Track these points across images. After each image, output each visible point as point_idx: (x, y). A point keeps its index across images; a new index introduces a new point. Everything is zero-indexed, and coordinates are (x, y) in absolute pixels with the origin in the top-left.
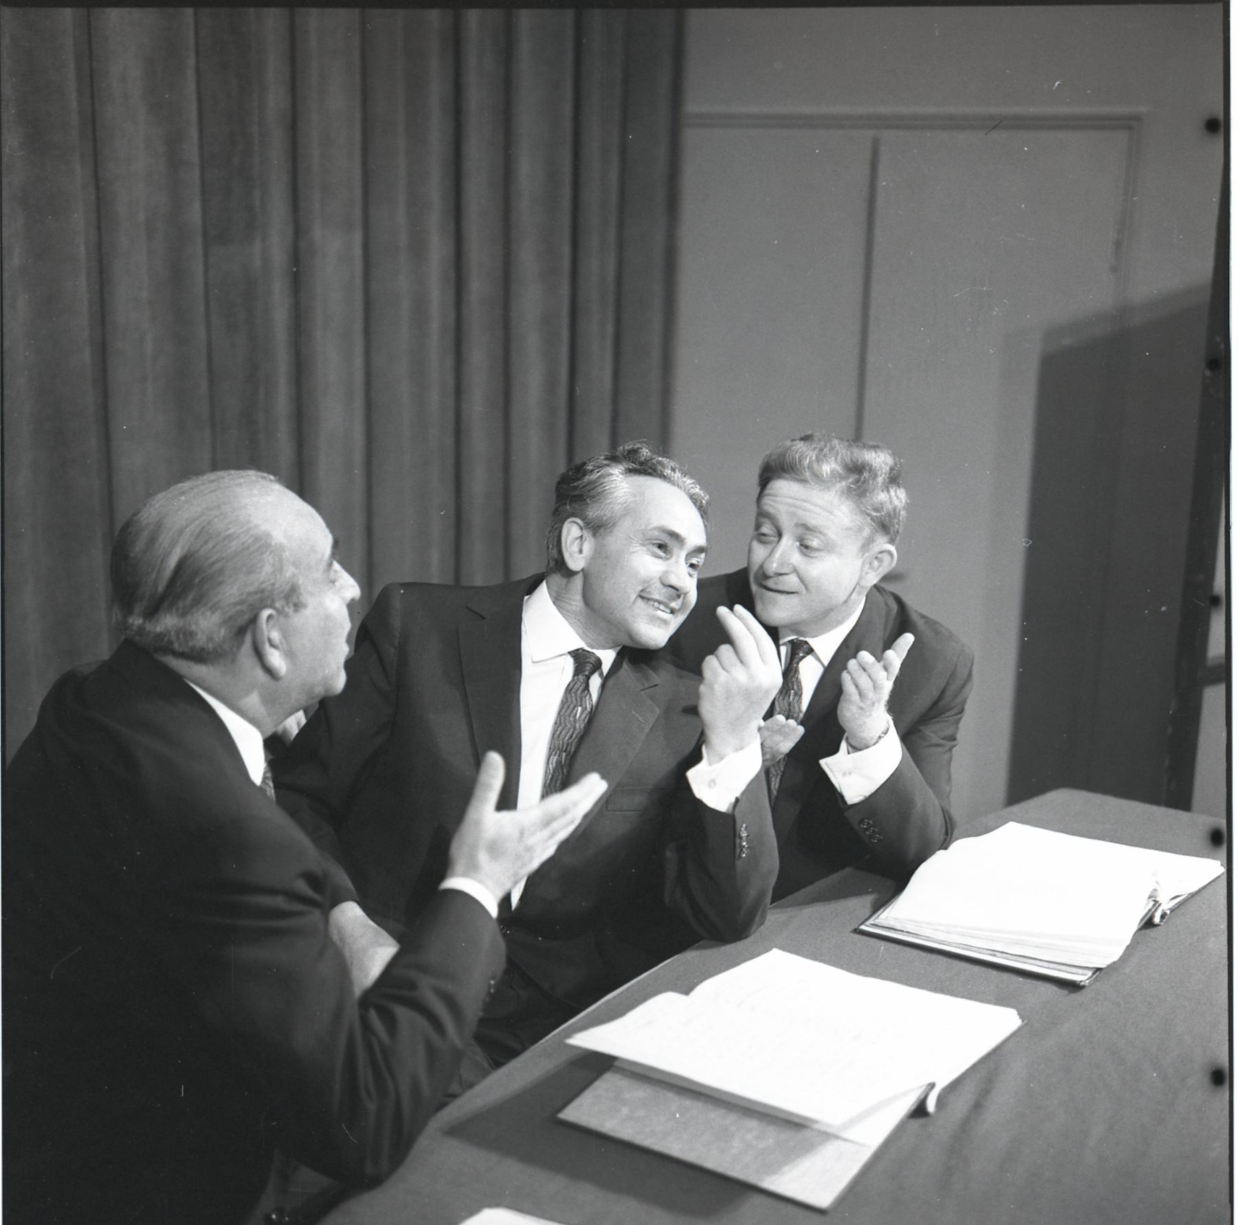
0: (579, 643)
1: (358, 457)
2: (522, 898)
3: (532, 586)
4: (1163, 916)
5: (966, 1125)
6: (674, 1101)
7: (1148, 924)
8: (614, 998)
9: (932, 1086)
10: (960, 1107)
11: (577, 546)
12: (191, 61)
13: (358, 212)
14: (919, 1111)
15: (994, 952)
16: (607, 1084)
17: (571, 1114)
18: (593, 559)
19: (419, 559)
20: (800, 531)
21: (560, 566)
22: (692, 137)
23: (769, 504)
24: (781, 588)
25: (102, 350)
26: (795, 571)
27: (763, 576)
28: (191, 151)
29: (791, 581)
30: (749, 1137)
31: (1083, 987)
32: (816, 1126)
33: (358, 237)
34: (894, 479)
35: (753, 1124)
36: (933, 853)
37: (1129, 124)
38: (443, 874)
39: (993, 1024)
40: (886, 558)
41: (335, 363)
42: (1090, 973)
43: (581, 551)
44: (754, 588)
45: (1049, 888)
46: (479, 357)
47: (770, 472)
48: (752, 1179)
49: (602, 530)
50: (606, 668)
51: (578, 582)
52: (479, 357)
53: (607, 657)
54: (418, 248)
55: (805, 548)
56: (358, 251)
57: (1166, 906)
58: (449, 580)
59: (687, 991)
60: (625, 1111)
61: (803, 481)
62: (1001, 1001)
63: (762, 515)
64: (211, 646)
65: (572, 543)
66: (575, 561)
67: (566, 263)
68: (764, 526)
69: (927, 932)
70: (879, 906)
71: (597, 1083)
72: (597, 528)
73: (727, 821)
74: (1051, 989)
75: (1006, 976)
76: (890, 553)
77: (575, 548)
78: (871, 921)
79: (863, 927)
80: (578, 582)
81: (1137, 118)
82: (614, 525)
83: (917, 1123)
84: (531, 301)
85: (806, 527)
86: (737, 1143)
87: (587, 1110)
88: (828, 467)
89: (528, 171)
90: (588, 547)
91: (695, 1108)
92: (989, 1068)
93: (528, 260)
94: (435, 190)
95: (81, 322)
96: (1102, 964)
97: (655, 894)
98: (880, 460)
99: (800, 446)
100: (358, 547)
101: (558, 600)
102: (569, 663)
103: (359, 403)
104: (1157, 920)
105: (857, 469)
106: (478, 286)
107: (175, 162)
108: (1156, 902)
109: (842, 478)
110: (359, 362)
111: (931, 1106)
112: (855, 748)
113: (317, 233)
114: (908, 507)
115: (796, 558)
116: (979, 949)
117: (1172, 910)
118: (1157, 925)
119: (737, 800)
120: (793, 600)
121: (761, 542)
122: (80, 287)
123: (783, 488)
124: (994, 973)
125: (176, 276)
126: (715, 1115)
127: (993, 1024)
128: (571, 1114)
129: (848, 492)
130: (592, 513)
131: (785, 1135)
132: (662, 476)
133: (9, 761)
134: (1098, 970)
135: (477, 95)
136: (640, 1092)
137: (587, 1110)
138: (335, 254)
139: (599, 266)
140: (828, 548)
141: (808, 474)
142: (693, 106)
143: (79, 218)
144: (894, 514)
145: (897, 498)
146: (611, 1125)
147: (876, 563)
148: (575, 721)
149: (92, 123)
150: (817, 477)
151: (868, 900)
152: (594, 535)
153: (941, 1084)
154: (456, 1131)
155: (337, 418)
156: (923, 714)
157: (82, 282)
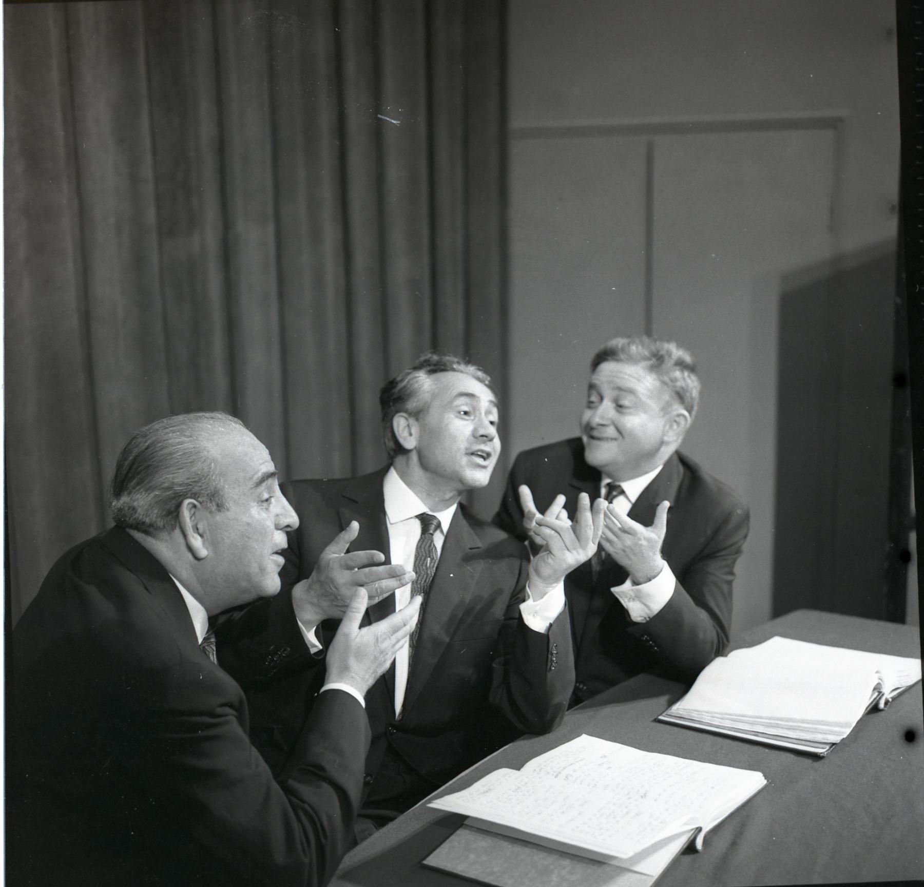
0: (422, 508)
1: (277, 387)
2: (404, 705)
4: (887, 703)
5: (725, 859)
6: (509, 849)
7: (874, 709)
8: (466, 775)
10: (722, 844)
11: (406, 431)
12: (145, 107)
13: (270, 210)
14: (690, 848)
15: (756, 733)
16: (461, 837)
17: (432, 860)
18: (420, 439)
19: (325, 462)
20: (615, 393)
21: (400, 450)
22: (518, 149)
25: (86, 317)
28: (147, 171)
30: (564, 872)
31: (823, 757)
32: (613, 862)
33: (271, 228)
35: (566, 862)
36: (712, 660)
37: (834, 124)
38: (322, 682)
40: (682, 421)
41: (257, 320)
42: (828, 747)
43: (411, 435)
45: (799, 684)
49: (421, 415)
50: (445, 526)
51: (414, 457)
53: (446, 517)
54: (316, 236)
56: (271, 239)
57: (888, 695)
58: (349, 476)
59: (518, 768)
60: (472, 856)
62: (751, 766)
64: (147, 520)
65: (403, 430)
66: (409, 442)
67: (425, 241)
69: (707, 719)
70: (672, 702)
71: (452, 837)
72: (417, 415)
73: (543, 639)
74: (791, 756)
75: (756, 748)
77: (406, 434)
78: (670, 712)
79: (661, 718)
80: (414, 457)
81: (841, 120)
83: (688, 858)
84: (403, 267)
85: (620, 389)
86: (554, 878)
87: (441, 858)
89: (395, 174)
90: (414, 430)
91: (525, 853)
92: (742, 815)
93: (398, 239)
94: (327, 193)
95: (70, 296)
96: (836, 739)
97: (491, 692)
101: (405, 477)
102: (417, 526)
103: (276, 348)
104: (882, 705)
106: (362, 260)
107: (134, 179)
108: (880, 692)
112: (635, 583)
113: (241, 226)
117: (894, 699)
118: (882, 710)
119: (551, 625)
122: (68, 270)
124: (747, 746)
125: (138, 261)
126: (541, 859)
128: (432, 860)
131: (591, 869)
132: (454, 370)
133: (15, 620)
134: (834, 744)
136: (484, 842)
137: (441, 858)
138: (255, 242)
139: (451, 241)
142: (516, 122)
143: (67, 223)
146: (460, 868)
148: (427, 569)
149: (75, 154)
151: (663, 700)
152: (417, 420)
153: (707, 827)
154: (348, 876)
155: (260, 362)
156: (693, 559)
157: (70, 266)
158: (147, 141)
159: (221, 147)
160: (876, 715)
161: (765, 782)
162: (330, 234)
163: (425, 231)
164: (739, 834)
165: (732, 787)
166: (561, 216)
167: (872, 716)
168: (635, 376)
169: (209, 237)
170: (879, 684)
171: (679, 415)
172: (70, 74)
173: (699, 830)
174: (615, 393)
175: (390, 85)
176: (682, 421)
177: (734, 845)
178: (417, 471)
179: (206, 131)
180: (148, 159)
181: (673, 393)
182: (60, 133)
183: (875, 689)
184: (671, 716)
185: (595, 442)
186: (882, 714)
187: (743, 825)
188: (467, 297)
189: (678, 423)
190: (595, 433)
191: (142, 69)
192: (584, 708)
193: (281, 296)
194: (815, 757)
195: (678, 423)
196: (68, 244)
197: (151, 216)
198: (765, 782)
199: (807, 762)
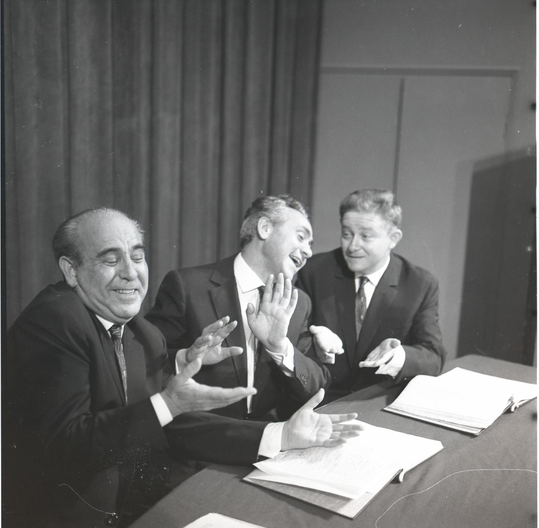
3: (236, 255)
4: (516, 408)
5: (415, 488)
7: (508, 411)
9: (402, 470)
10: (414, 479)
14: (396, 480)
15: (440, 421)
18: (272, 235)
20: (361, 231)
22: (326, 80)
23: (346, 222)
24: (358, 255)
25: (69, 161)
26: (362, 248)
27: (349, 252)
28: (109, 79)
29: (361, 252)
31: (476, 436)
33: (178, 117)
34: (395, 203)
39: (430, 447)
40: (397, 235)
41: (167, 170)
42: (480, 430)
43: (266, 231)
44: (346, 257)
45: (467, 395)
46: (230, 169)
47: (345, 208)
48: (334, 510)
52: (230, 169)
55: (364, 236)
56: (178, 122)
57: (517, 404)
61: (358, 211)
63: (344, 227)
68: (345, 231)
72: (275, 223)
76: (399, 233)
78: (391, 406)
79: (385, 409)
82: (284, 222)
83: (394, 486)
84: (253, 144)
85: (364, 229)
88: (367, 205)
89: (253, 89)
90: (270, 230)
93: (251, 127)
94: (212, 98)
96: (486, 427)
98: (388, 197)
99: (354, 197)
100: (150, 248)
104: (513, 409)
105: (381, 203)
106: (230, 138)
108: (512, 402)
109: (374, 207)
110: (177, 168)
111: (401, 478)
113: (161, 114)
114: (403, 214)
115: (361, 243)
116: (434, 419)
117: (520, 406)
120: (363, 260)
121: (345, 238)
123: (352, 216)
127: (430, 447)
129: (377, 212)
130: (273, 215)
134: (483, 429)
135: (232, 58)
140: (374, 236)
141: (359, 208)
142: (325, 64)
143: (60, 106)
144: (397, 218)
145: (397, 211)
147: (394, 238)
150: (364, 209)
152: (274, 226)
158: (110, 62)
159: (152, 67)
160: (509, 415)
161: (443, 447)
162: (213, 121)
163: (268, 124)
164: (424, 475)
165: (423, 449)
166: (348, 118)
167: (507, 415)
168: (374, 221)
169: (142, 119)
170: (512, 397)
171: (396, 233)
172: (67, 22)
173: (402, 470)
174: (361, 231)
175: (252, 38)
176: (397, 235)
177: (421, 480)
178: (258, 257)
179: (144, 58)
180: (110, 72)
181: (392, 223)
182: (60, 56)
183: (509, 400)
184: (391, 408)
185: (353, 259)
186: (513, 414)
187: (427, 470)
188: (290, 164)
189: (395, 237)
190: (353, 255)
191: (109, 19)
192: (342, 401)
193: (182, 157)
194: (472, 436)
195: (395, 237)
196: (61, 118)
197: (109, 105)
198: (443, 447)
199: (468, 438)
